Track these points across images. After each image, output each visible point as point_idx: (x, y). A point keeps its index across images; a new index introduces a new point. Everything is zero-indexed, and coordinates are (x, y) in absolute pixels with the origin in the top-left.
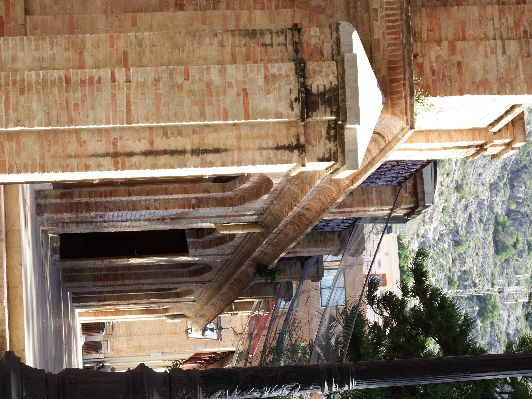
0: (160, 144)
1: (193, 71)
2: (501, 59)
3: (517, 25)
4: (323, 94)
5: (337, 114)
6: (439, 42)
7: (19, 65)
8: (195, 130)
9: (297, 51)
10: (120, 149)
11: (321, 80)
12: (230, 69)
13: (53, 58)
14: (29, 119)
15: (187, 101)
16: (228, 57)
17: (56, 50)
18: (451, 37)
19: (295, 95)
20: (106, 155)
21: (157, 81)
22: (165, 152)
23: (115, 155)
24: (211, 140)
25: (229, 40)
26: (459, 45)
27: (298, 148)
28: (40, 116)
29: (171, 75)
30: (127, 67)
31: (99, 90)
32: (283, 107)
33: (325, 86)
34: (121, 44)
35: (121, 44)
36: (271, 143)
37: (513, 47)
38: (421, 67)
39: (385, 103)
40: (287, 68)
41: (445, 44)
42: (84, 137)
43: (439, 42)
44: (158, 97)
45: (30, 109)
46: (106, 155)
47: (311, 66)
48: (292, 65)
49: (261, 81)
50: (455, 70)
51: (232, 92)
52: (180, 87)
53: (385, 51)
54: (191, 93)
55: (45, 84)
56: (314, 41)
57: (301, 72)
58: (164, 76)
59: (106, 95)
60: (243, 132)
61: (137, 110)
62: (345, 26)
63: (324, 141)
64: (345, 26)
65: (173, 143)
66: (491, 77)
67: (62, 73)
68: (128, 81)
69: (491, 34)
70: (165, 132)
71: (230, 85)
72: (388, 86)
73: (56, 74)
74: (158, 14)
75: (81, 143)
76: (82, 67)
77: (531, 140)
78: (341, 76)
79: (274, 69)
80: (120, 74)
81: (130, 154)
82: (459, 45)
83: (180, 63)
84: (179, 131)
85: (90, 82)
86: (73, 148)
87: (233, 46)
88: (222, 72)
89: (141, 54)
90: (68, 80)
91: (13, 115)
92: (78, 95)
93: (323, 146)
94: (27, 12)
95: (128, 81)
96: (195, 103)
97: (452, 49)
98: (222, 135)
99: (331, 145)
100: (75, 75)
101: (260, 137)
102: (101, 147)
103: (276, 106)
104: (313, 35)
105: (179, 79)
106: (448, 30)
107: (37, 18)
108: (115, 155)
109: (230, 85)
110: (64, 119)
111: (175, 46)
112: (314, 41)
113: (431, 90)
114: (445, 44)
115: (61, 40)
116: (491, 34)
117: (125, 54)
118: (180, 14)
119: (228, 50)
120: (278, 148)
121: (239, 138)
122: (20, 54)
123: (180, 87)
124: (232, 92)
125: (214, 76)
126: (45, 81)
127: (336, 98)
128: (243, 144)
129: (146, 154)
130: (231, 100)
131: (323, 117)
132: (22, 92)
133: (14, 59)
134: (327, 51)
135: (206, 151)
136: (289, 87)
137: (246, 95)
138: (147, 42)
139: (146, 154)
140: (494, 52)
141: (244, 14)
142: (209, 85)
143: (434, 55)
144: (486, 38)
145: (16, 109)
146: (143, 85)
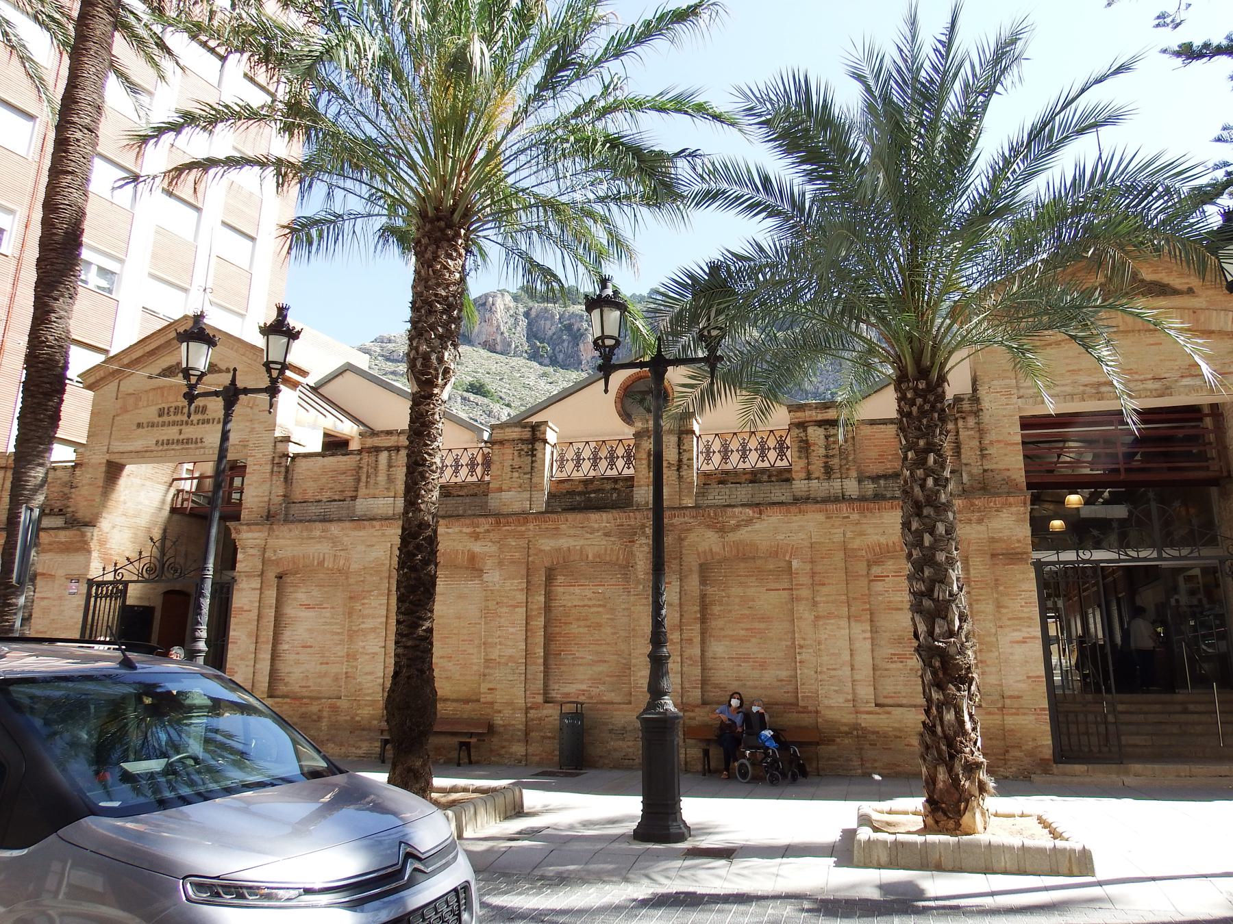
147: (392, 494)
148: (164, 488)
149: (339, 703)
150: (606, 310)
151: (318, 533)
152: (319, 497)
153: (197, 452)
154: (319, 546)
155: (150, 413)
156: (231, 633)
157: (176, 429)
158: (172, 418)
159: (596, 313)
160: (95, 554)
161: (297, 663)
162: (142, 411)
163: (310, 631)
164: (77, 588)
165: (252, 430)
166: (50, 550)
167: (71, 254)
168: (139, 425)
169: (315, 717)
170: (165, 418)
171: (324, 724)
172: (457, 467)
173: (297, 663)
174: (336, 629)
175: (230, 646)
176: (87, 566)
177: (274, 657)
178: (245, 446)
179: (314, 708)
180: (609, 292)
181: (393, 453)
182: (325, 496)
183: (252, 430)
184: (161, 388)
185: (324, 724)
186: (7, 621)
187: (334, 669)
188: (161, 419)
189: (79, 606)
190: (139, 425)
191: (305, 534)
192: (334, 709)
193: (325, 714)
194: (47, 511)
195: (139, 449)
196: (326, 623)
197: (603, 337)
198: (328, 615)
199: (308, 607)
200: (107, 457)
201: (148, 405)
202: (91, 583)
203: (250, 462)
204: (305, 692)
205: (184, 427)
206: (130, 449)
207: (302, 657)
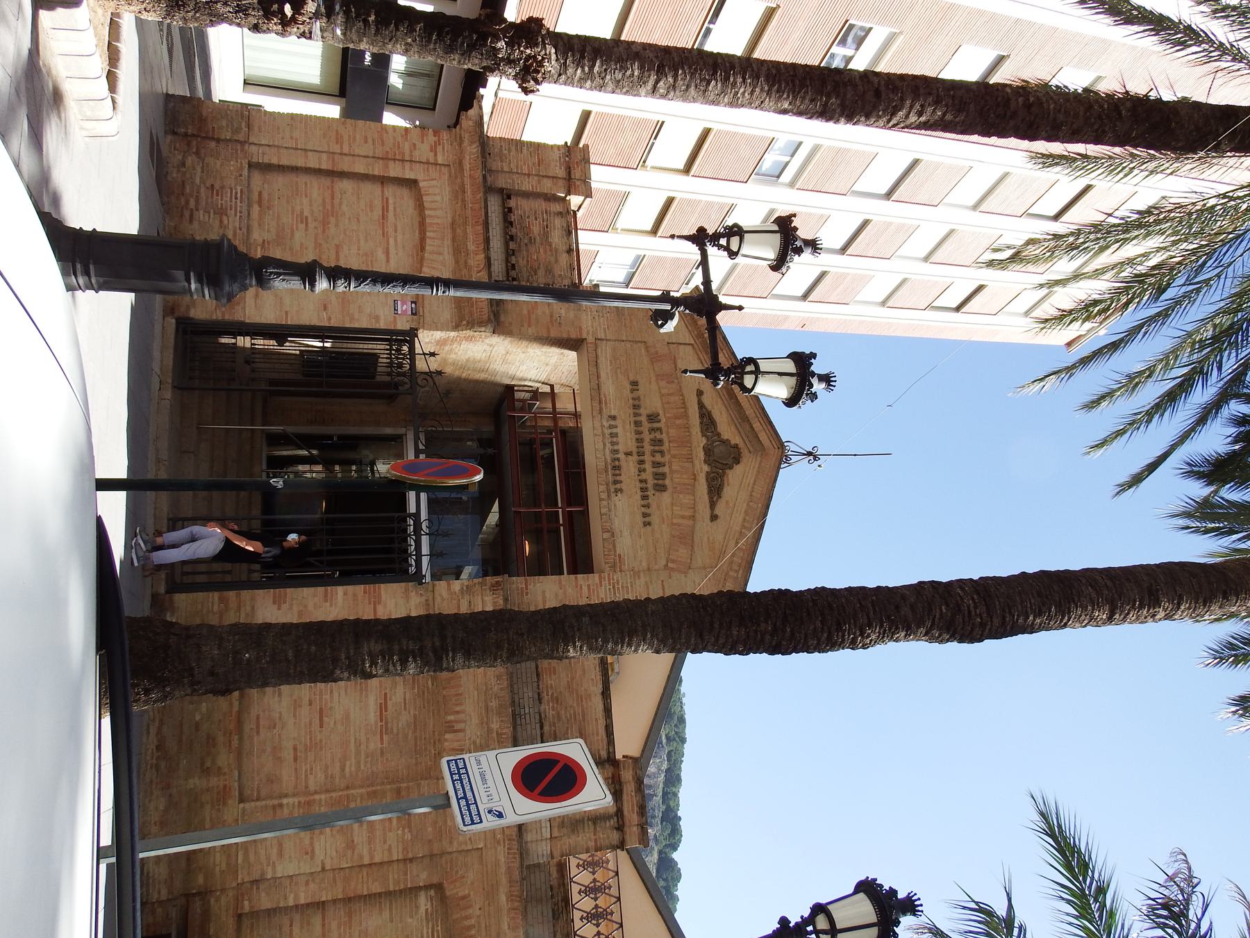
147: (556, 834)
148: (542, 378)
149: (232, 802)
150: (793, 381)
151: (495, 726)
152: (545, 698)
153: (602, 488)
154: (475, 721)
155: (652, 403)
156: (340, 590)
157: (632, 445)
158: (647, 437)
159: (790, 367)
160: (453, 334)
161: (296, 705)
162: (654, 386)
163: (347, 717)
164: (404, 312)
165: (636, 574)
166: (457, 262)
167: (841, 116)
168: (635, 383)
169: (208, 764)
170: (646, 426)
171: (196, 782)
172: (593, 890)
173: (296, 705)
174: (350, 767)
175: (321, 590)
176: (436, 327)
177: (294, 169)
178: (613, 567)
179: (224, 759)
180: (818, 387)
181: (613, 822)
182: (547, 708)
183: (636, 574)
184: (685, 415)
185: (196, 782)
186: (374, 663)
187: (287, 777)
188: (643, 419)
189: (377, 318)
190: (635, 383)
191: (494, 704)
192: (222, 796)
193: (214, 781)
194: (512, 245)
195: (603, 389)
196: (358, 744)
197: (757, 372)
198: (372, 746)
199: (383, 708)
200: (590, 339)
201: (662, 395)
202: (411, 335)
203: (594, 578)
204: (248, 726)
205: (635, 458)
206: (603, 375)
207: (305, 711)
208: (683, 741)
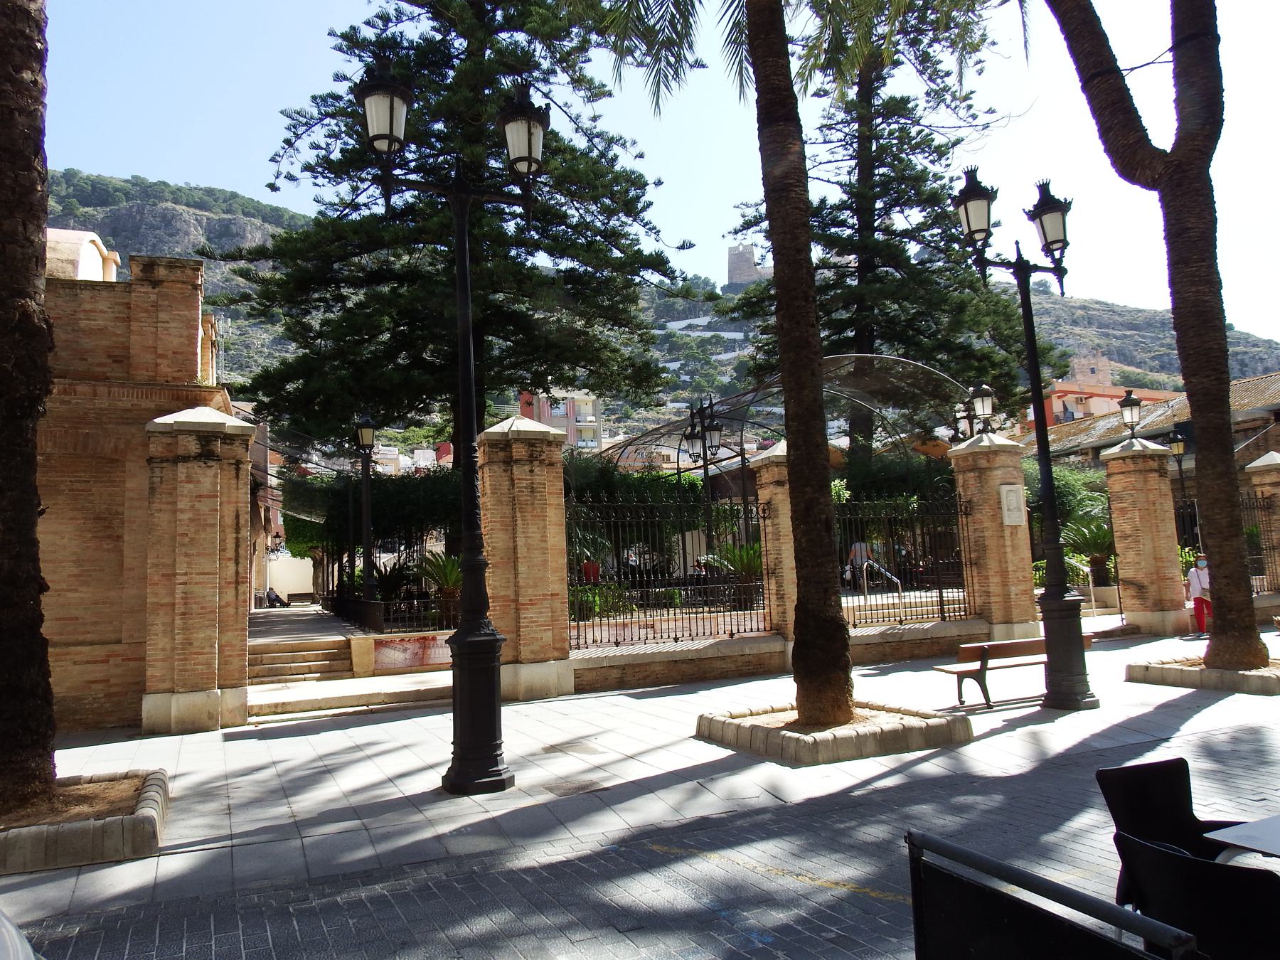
0: (230, 553)
1: (180, 530)
2: (172, 325)
3: (146, 311)
4: (202, 446)
5: (217, 437)
6: (157, 365)
7: (168, 646)
8: (222, 531)
9: (167, 461)
10: (233, 580)
11: (193, 447)
12: (180, 505)
13: (164, 624)
14: (210, 638)
15: (203, 535)
16: (169, 507)
17: (158, 623)
18: (153, 356)
19: (202, 464)
20: (236, 589)
21: (186, 555)
22: (237, 551)
23: (237, 583)
24: (229, 520)
25: (156, 506)
26: (160, 351)
27: (238, 464)
28: (208, 632)
29: (184, 545)
30: (175, 575)
31: (192, 593)
32: (211, 472)
33: (376, 463)
34: (156, 578)
35: (156, 578)
36: (234, 482)
37: (163, 316)
38: (174, 379)
39: (206, 405)
40: (182, 469)
41: (159, 361)
42: (223, 603)
43: (157, 365)
44: (199, 555)
45: (204, 639)
46: (236, 589)
47: (181, 451)
48: (180, 465)
49: (191, 486)
50: (179, 356)
51: (197, 505)
52: (192, 539)
53: (164, 402)
54: (197, 532)
55: (185, 629)
56: (160, 449)
57: (186, 459)
58: (184, 550)
59: (196, 589)
60: (225, 499)
61: (207, 567)
62: (149, 427)
63: (234, 447)
64: (149, 427)
65: (230, 545)
66: (185, 333)
67: (177, 618)
68: (186, 574)
69: (153, 329)
70: (223, 550)
71: (193, 506)
72: (193, 403)
73: (178, 622)
74: (125, 553)
75: (228, 605)
76: (173, 605)
77: (1275, 536)
78: (189, 433)
79: (182, 476)
80: (180, 579)
81: (237, 573)
82: (160, 351)
83: (174, 538)
84: (223, 541)
85: (186, 597)
86: (231, 611)
87: (161, 503)
88: (182, 511)
89: (164, 565)
90: (184, 614)
91: (207, 650)
92: (194, 606)
93: (238, 449)
94: (119, 642)
95: (186, 574)
96: (205, 530)
97: (162, 356)
98: (226, 512)
99: (237, 443)
100: (179, 609)
101: (229, 489)
102: (230, 593)
103: (208, 477)
104: (155, 448)
105: (187, 540)
106: (149, 358)
107: (124, 635)
108: (237, 583)
109: (193, 506)
110: (212, 616)
111: (159, 541)
112: (160, 449)
113: (193, 375)
114: (159, 361)
115: (150, 618)
116: (153, 329)
117: (163, 575)
118: (126, 538)
119: (163, 507)
120: (237, 477)
121: (229, 502)
122: (160, 646)
123: (192, 539)
124: (197, 505)
125: (185, 516)
126: (183, 629)
127: (205, 437)
128: (233, 500)
129: (237, 563)
130: (204, 507)
131: (218, 447)
132: (191, 644)
133: (163, 650)
134: (169, 440)
135: (238, 524)
136: (196, 468)
137: (201, 496)
138: (155, 561)
139: (237, 563)
140: (166, 329)
141: (128, 494)
142: (191, 520)
143: (165, 368)
144: (156, 333)
145: (203, 648)
146: (189, 564)
208: (234, 195)
